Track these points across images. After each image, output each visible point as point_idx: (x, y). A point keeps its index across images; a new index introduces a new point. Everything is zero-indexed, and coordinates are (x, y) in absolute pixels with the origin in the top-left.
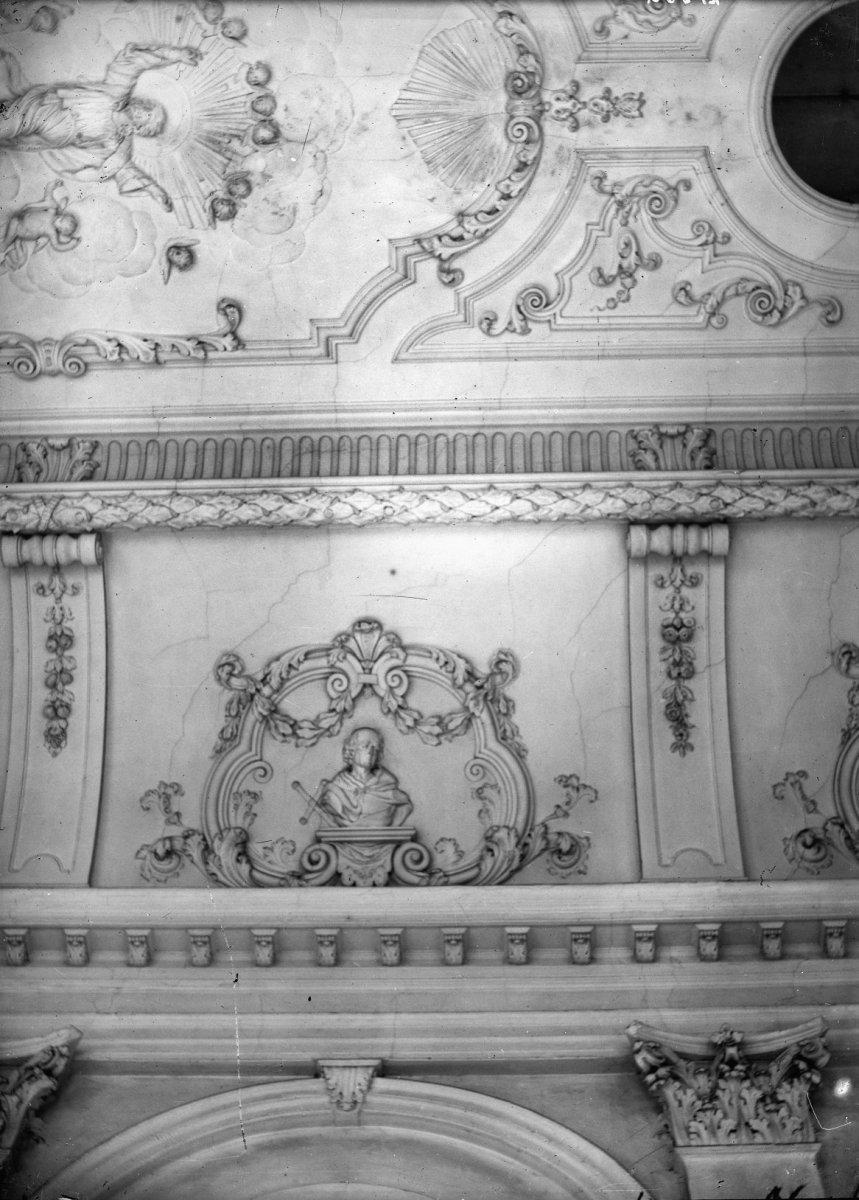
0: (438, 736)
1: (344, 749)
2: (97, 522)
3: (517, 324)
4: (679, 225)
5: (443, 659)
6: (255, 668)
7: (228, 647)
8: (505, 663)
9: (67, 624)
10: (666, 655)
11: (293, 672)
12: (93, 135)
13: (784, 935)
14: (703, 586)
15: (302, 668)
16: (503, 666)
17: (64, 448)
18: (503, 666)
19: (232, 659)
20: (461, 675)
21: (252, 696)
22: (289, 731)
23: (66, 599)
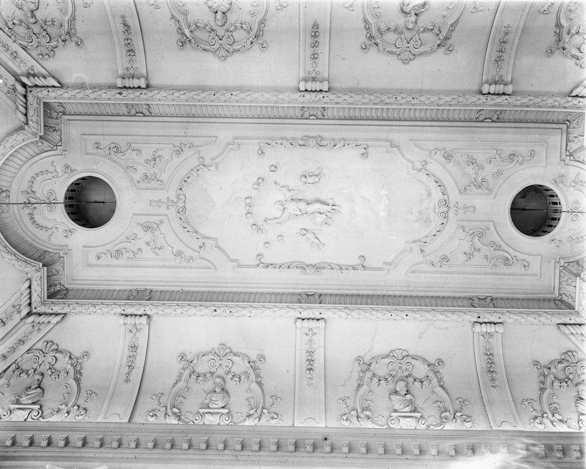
0: (198, 23)
1: (227, 19)
2: (299, 94)
3: (183, 146)
4: (141, 170)
5: (199, 47)
6: (256, 47)
7: (85, 350)
8: (440, 361)
9: (312, 62)
10: (133, 46)
11: (243, 44)
12: (432, 363)
13: (323, 202)
14: (125, 68)
15: (241, 46)
16: (181, 44)
17: (311, 116)
18: (181, 44)
19: (263, 49)
20: (193, 41)
21: (255, 37)
22: (244, 26)
23: (312, 70)
